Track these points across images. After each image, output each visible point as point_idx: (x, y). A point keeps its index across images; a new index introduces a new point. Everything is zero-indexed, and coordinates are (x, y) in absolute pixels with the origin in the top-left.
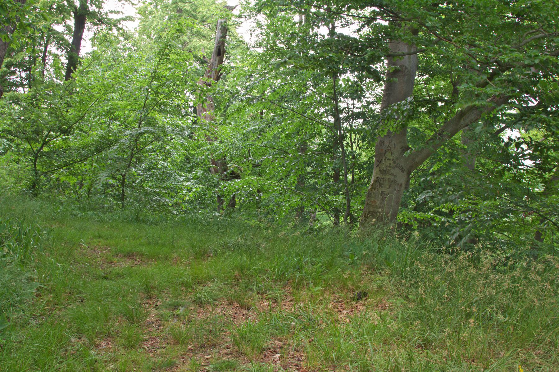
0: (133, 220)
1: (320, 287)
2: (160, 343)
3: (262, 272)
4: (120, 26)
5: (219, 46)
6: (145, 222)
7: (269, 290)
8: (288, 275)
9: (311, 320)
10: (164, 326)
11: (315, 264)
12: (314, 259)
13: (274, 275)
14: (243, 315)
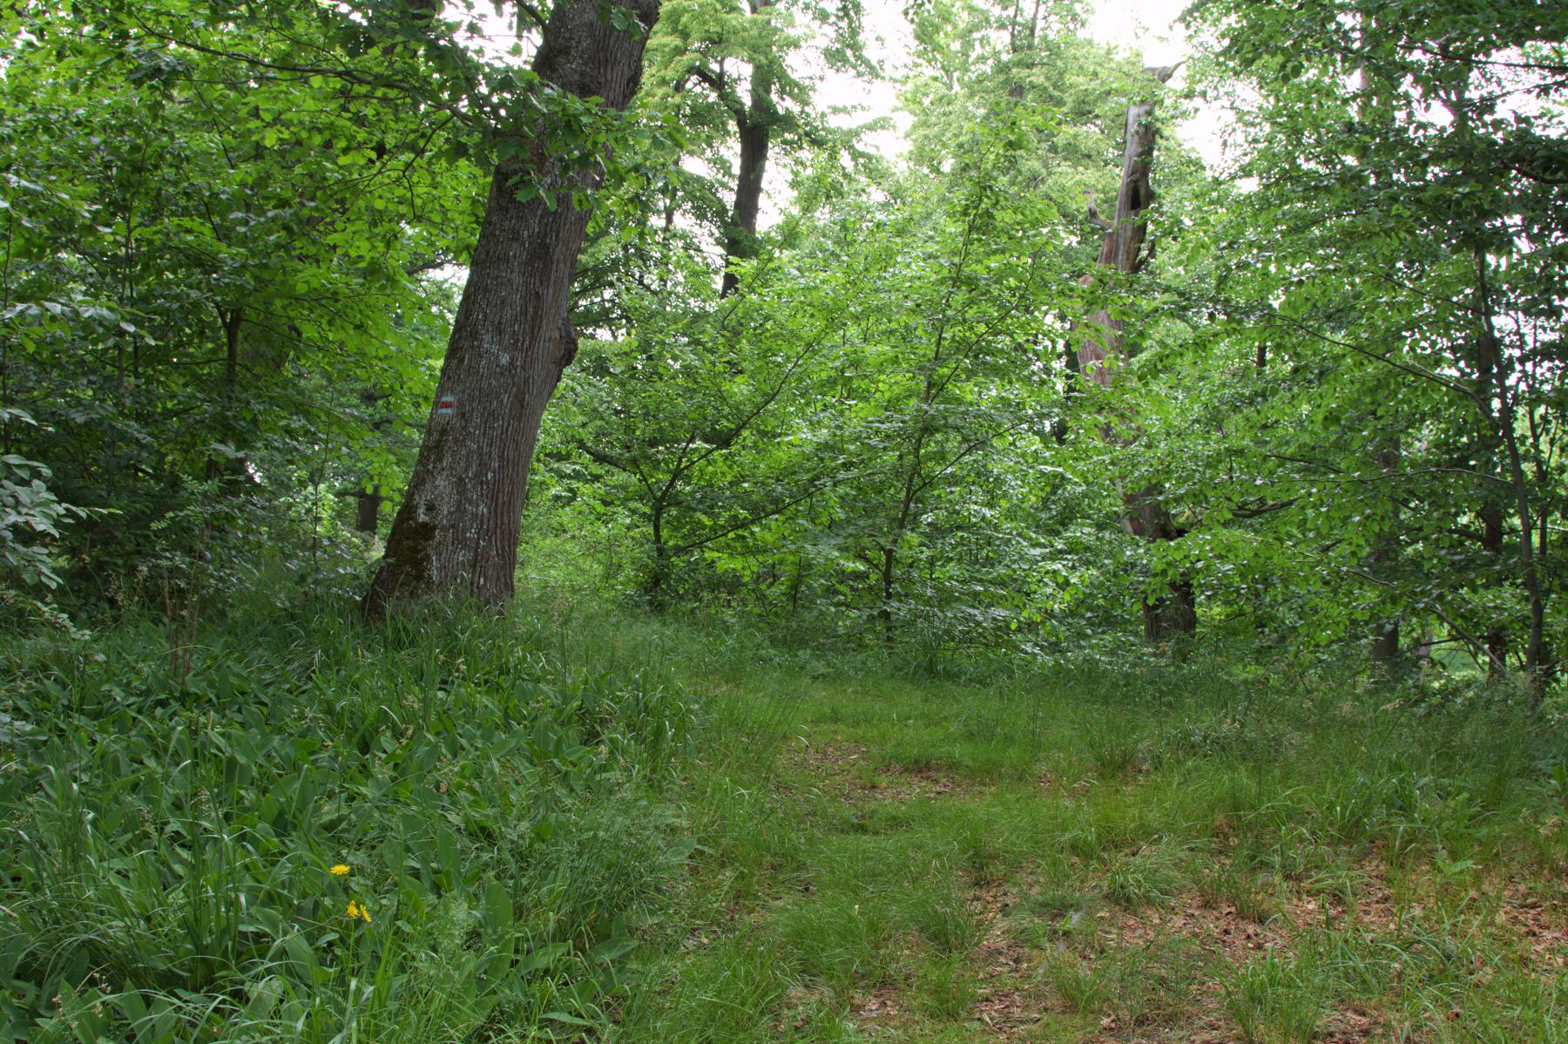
0: (921, 671)
1: (1470, 863)
2: (1025, 1008)
3: (1295, 815)
4: (860, 147)
5: (1135, 182)
6: (952, 676)
7: (1317, 867)
8: (1372, 825)
9: (1449, 957)
10: (1030, 961)
11: (1449, 794)
12: (1445, 781)
13: (1331, 824)
14: (1249, 937)
